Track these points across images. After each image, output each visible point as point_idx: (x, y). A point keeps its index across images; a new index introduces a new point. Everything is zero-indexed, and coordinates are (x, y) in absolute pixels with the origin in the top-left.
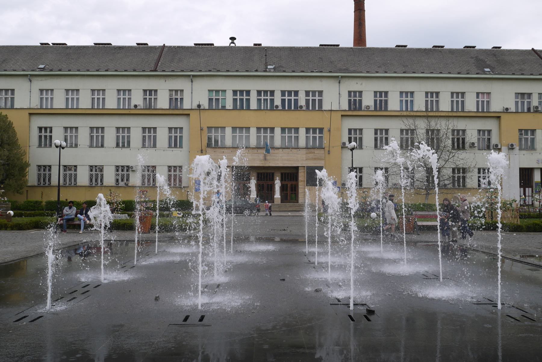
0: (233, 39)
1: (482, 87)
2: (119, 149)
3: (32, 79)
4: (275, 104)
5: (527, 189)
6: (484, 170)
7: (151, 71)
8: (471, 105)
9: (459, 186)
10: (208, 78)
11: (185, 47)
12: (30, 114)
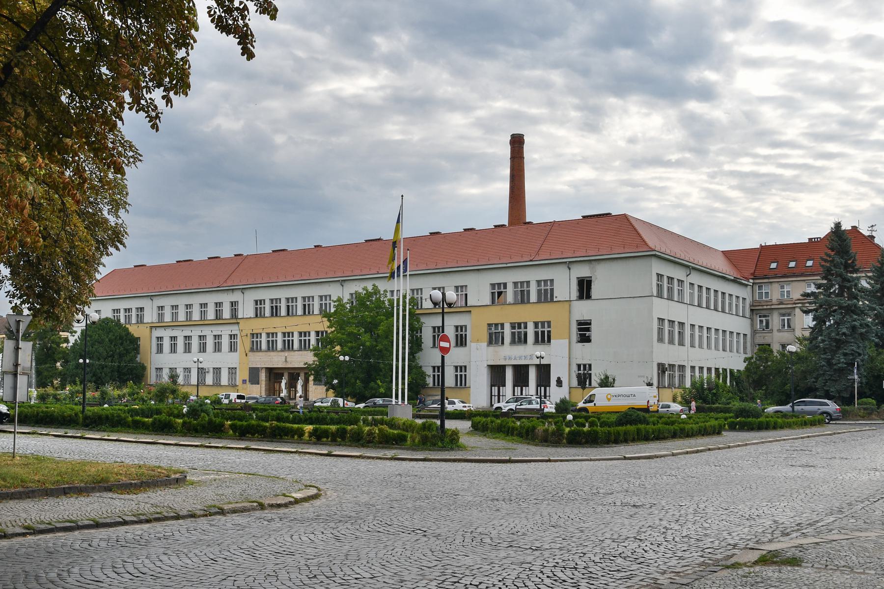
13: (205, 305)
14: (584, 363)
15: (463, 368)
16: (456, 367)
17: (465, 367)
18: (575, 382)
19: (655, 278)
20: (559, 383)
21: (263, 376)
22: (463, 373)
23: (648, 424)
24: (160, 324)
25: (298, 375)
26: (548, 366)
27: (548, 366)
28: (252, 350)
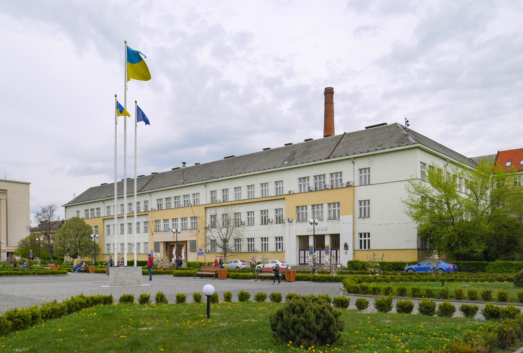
0: (184, 163)
1: (277, 177)
2: (361, 219)
3: (105, 202)
4: (326, 184)
5: (322, 251)
6: (265, 238)
7: (325, 159)
8: (272, 192)
9: (365, 248)
10: (361, 159)
11: (215, 162)
12: (104, 219)
13: (266, 184)
14: (365, 232)
15: (280, 238)
16: (249, 239)
17: (282, 237)
18: (357, 247)
19: (419, 165)
20: (346, 247)
21: (162, 247)
22: (266, 243)
23: (102, 267)
24: (214, 204)
25: (174, 246)
26: (338, 235)
27: (338, 235)
28: (156, 231)
